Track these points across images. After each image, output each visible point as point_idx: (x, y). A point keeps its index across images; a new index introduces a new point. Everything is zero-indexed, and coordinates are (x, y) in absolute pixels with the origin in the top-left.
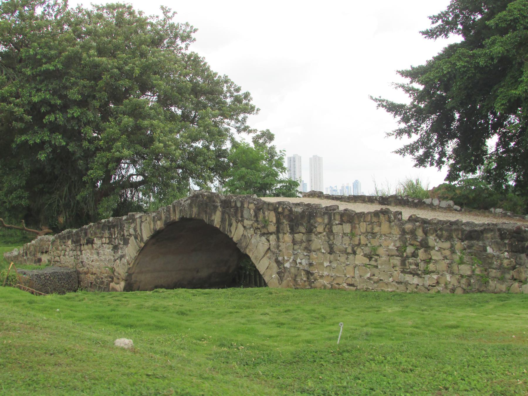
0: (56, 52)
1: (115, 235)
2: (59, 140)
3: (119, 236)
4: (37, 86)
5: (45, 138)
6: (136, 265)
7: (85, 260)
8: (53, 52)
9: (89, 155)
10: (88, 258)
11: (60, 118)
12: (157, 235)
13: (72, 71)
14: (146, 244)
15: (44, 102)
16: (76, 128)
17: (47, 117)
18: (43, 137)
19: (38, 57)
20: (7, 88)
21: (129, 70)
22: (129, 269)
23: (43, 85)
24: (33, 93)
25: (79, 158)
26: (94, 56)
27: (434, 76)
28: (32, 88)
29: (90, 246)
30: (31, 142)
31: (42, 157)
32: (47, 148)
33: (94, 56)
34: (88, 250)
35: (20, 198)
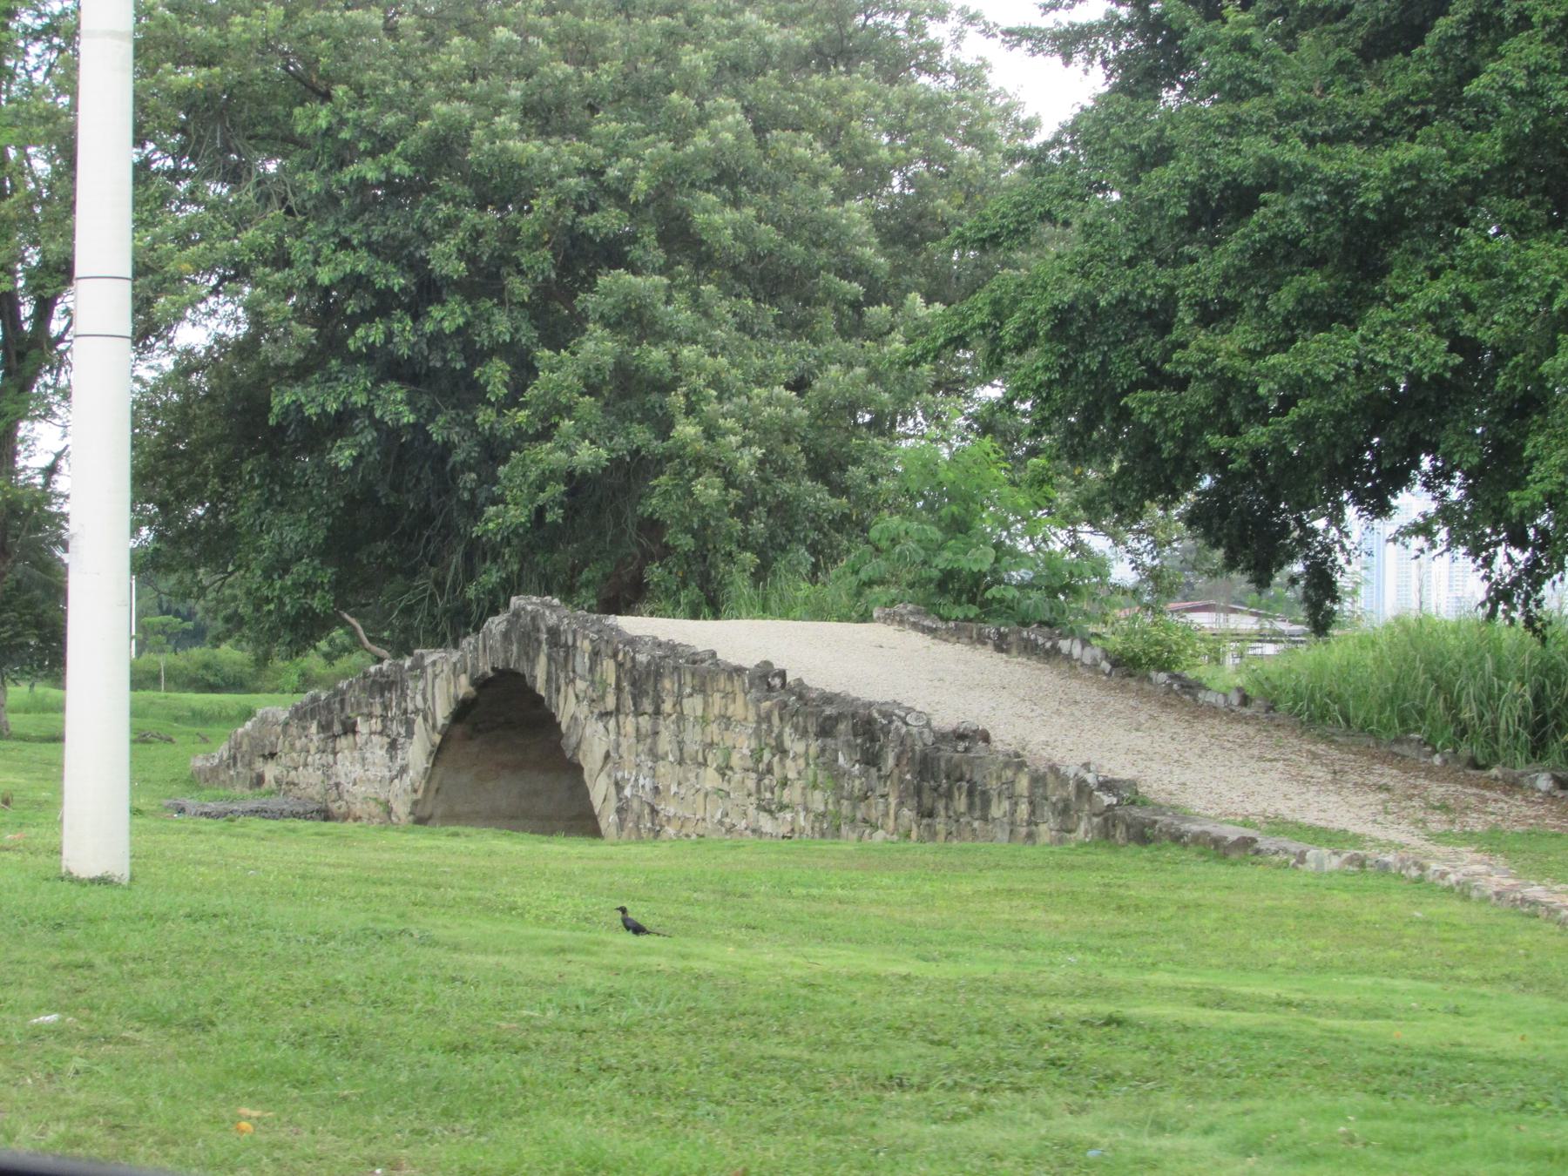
0: (402, 116)
2: (396, 405)
4: (341, 230)
5: (354, 399)
6: (432, 793)
7: (343, 780)
8: (390, 119)
9: (494, 451)
11: (404, 334)
12: (463, 711)
13: (442, 182)
14: (446, 736)
15: (355, 283)
16: (458, 366)
17: (360, 332)
18: (350, 395)
19: (345, 134)
21: (619, 179)
22: (415, 803)
23: (358, 226)
24: (326, 252)
25: (466, 466)
26: (507, 134)
27: (924, 347)
28: (325, 237)
29: (350, 737)
30: (311, 411)
31: (343, 456)
32: (362, 431)
33: (507, 134)
35: (309, 587)
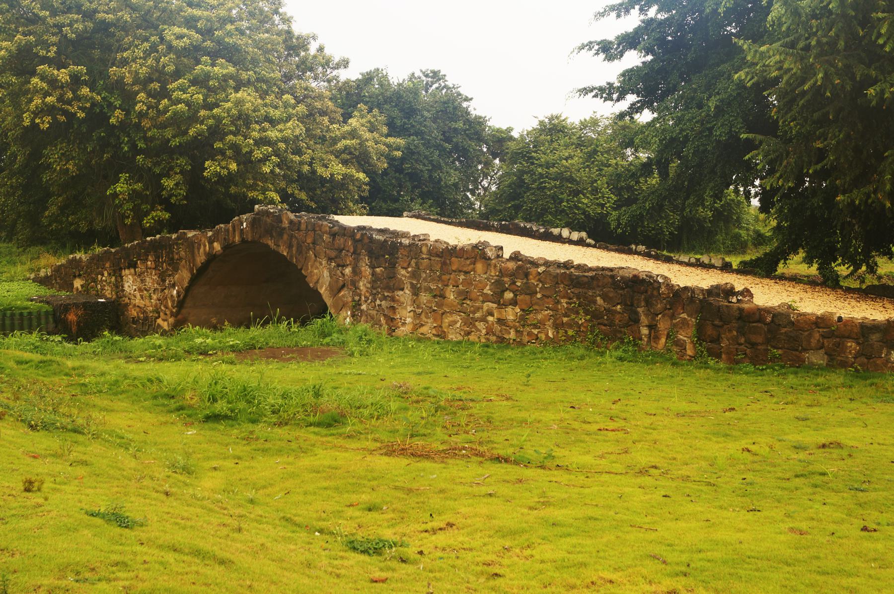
29: (132, 270)
34: (130, 277)
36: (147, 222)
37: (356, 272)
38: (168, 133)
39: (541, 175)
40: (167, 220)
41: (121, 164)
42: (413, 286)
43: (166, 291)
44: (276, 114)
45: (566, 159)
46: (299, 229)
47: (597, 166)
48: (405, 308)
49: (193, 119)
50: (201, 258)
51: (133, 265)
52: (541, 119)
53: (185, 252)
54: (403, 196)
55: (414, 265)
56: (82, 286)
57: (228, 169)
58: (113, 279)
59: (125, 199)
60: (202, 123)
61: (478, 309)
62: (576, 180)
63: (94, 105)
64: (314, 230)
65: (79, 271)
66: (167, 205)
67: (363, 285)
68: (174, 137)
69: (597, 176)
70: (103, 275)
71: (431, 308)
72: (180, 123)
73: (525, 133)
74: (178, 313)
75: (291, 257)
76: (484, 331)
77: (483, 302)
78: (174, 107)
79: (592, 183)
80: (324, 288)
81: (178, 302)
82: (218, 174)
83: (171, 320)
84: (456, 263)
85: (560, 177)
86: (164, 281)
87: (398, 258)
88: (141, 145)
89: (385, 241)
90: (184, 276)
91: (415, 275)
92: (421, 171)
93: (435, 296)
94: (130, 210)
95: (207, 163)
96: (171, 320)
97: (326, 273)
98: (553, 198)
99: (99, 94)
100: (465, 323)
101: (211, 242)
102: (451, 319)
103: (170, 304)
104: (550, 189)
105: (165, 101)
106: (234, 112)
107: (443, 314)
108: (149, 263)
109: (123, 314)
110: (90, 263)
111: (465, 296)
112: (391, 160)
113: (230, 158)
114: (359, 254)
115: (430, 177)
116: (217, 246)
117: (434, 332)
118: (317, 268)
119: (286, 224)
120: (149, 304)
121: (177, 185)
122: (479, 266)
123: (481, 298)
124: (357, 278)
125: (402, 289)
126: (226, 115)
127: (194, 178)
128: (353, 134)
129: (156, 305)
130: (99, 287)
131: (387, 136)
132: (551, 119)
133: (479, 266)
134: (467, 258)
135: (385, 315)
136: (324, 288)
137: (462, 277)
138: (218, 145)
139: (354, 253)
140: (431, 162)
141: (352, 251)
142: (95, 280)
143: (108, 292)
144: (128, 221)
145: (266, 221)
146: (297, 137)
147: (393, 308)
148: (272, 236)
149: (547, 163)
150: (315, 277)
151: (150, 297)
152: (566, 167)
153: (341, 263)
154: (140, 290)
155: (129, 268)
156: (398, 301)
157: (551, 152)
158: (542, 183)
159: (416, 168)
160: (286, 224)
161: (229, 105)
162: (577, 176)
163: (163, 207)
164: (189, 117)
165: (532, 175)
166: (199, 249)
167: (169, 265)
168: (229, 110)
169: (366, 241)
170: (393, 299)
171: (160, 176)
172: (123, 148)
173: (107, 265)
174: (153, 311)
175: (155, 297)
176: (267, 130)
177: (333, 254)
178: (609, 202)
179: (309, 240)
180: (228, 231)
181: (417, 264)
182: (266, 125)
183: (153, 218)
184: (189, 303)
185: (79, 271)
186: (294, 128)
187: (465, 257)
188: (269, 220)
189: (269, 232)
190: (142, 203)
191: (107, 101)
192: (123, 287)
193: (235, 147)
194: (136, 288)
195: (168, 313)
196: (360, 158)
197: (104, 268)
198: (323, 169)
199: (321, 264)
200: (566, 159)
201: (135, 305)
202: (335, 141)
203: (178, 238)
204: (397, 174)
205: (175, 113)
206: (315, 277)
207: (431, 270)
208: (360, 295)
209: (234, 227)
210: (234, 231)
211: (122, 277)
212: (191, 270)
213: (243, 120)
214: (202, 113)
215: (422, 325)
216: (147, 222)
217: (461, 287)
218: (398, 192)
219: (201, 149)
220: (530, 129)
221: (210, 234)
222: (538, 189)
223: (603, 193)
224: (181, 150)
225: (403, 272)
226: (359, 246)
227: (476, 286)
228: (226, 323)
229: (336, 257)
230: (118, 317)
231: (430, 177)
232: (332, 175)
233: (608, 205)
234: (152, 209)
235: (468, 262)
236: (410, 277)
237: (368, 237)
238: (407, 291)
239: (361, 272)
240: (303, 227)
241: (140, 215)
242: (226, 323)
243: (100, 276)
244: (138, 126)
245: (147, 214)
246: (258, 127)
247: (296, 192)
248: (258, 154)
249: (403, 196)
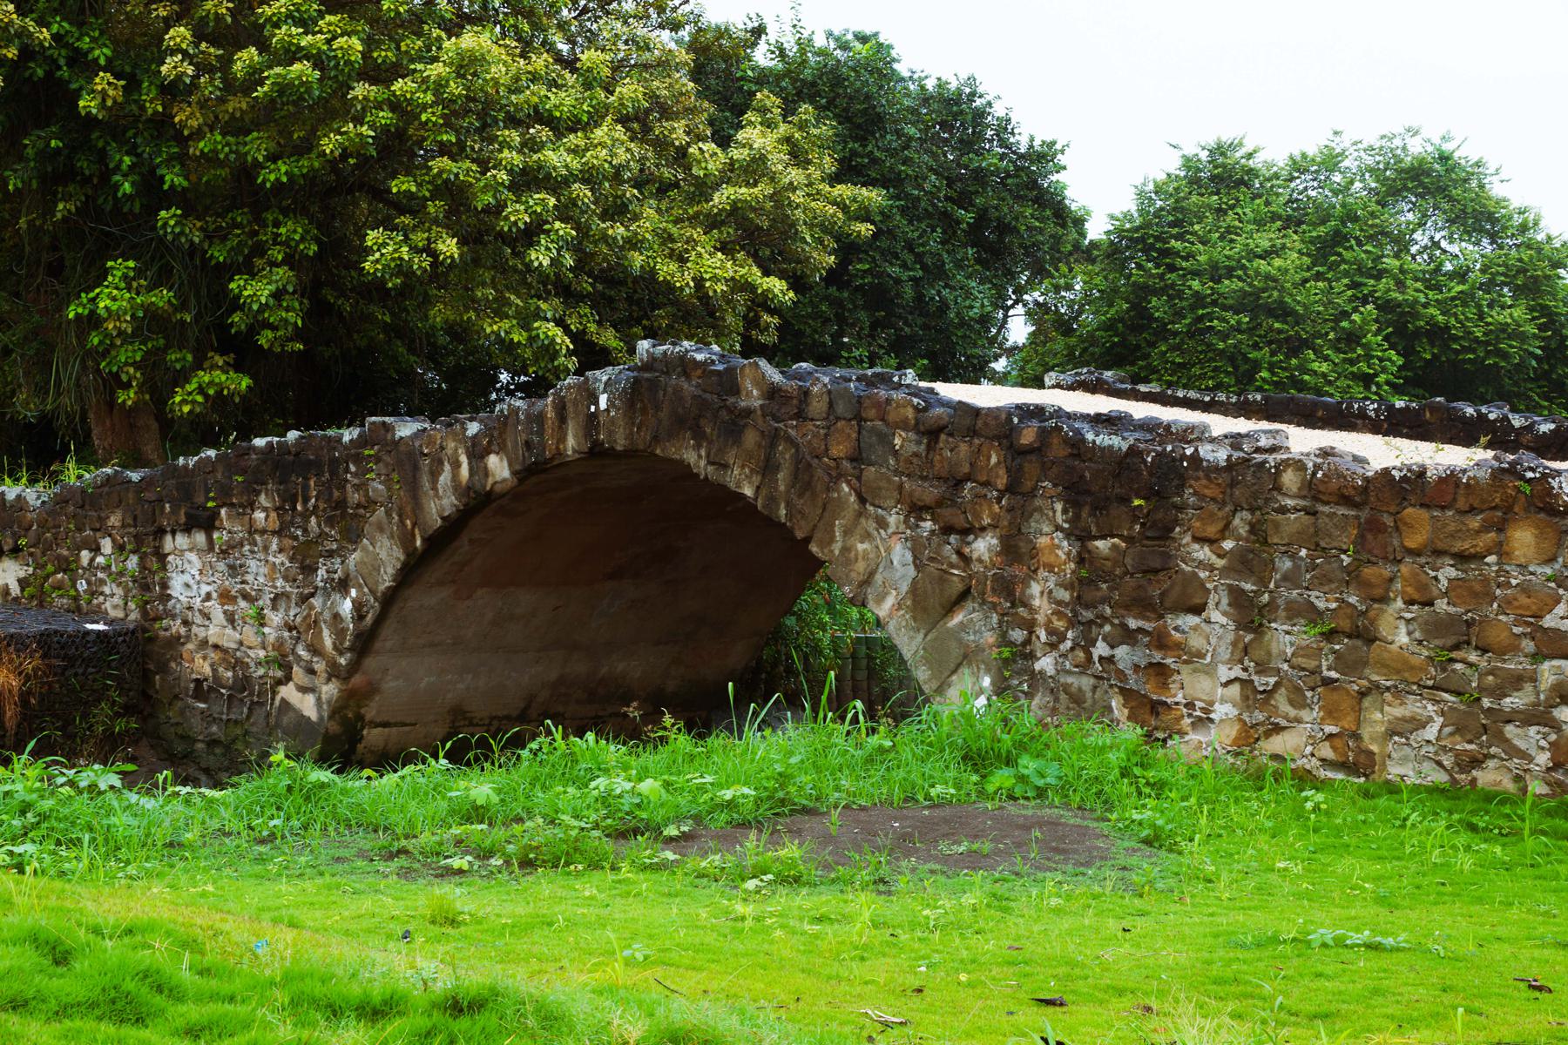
1: (306, 500)
3: (322, 506)
10: (187, 585)
20: (1036, 294)
29: (200, 538)
34: (193, 556)
36: (184, 401)
37: (1015, 549)
38: (257, 146)
39: (1199, 299)
40: (243, 398)
41: (107, 232)
42: (1239, 600)
43: (317, 602)
44: (563, 101)
45: (1266, 255)
46: (801, 415)
47: (1346, 274)
48: (1210, 671)
49: (334, 107)
50: (441, 502)
51: (208, 523)
52: (1190, 150)
53: (388, 482)
54: (848, 347)
55: (1243, 531)
56: (23, 583)
57: (434, 254)
58: (133, 562)
59: (121, 333)
60: (358, 120)
61: (1517, 681)
62: (1293, 313)
63: (27, 53)
64: (859, 418)
65: (16, 537)
66: (242, 352)
67: (1041, 594)
68: (273, 158)
69: (1350, 300)
70: (96, 550)
71: (1315, 672)
72: (299, 118)
73: (1151, 187)
74: (354, 667)
75: (772, 500)
76: (1543, 759)
77: (1538, 657)
78: (278, 70)
79: (1337, 320)
80: (890, 601)
81: (358, 636)
82: (402, 269)
83: (330, 690)
84: (1419, 526)
85: (1249, 303)
86: (309, 570)
87: (1181, 508)
88: (173, 178)
89: (1133, 451)
90: (382, 555)
91: (1247, 563)
92: (898, 281)
93: (1330, 636)
94: (134, 364)
95: (372, 236)
96: (330, 690)
97: (900, 554)
98: (1232, 360)
99: (41, 23)
100: (1460, 725)
101: (478, 453)
102: (1398, 712)
103: (328, 641)
104: (1224, 337)
105: (248, 56)
106: (455, 88)
107: (1362, 694)
108: (259, 516)
109: (164, 669)
110: (52, 513)
111: (1457, 635)
112: (848, 249)
113: (436, 222)
114: (1032, 494)
115: (920, 297)
116: (499, 467)
117: (1327, 751)
118: (867, 536)
119: (752, 397)
120: (254, 644)
121: (277, 295)
122: (1523, 538)
123: (1528, 646)
124: (1018, 571)
125: (1198, 610)
126: (429, 98)
127: (328, 273)
128: (755, 169)
129: (279, 645)
130: (82, 585)
131: (835, 179)
132: (1219, 150)
133: (1523, 538)
134: (1472, 510)
135: (1127, 693)
136: (890, 601)
137: (1447, 573)
138: (401, 185)
139: (1010, 489)
140: (919, 258)
141: (1002, 481)
142: (67, 566)
143: (118, 603)
144: (127, 397)
145: (678, 391)
146: (618, 170)
147: (1161, 672)
148: (699, 436)
149: (1214, 266)
150: (861, 566)
151: (261, 620)
152: (1268, 277)
153: (959, 521)
154: (226, 597)
155: (187, 530)
156: (1179, 647)
157: (1222, 238)
158: (1200, 319)
159: (881, 275)
160: (752, 397)
161: (436, 70)
162: (1298, 300)
163: (231, 358)
164: (323, 102)
165: (1171, 298)
166: (435, 475)
167: (331, 522)
168: (439, 86)
169: (1058, 450)
170: (1161, 641)
171: (226, 271)
172: (117, 186)
173: (114, 520)
174: (268, 662)
175: (275, 618)
176: (542, 146)
177: (930, 492)
178: (1384, 370)
179: (839, 449)
180: (540, 418)
181: (1253, 529)
182: (542, 133)
183: (201, 390)
184: (389, 637)
185: (16, 537)
186: (610, 145)
187: (1462, 503)
188: (689, 388)
189: (689, 422)
190: (167, 347)
191: (67, 45)
192: (165, 585)
193: (454, 193)
194: (218, 596)
195: (320, 666)
196: (758, 235)
197: (102, 529)
198: (673, 266)
199: (882, 524)
200: (1266, 255)
201: (204, 643)
202: (704, 188)
203: (362, 442)
204: (833, 290)
205: (283, 88)
206: (861, 566)
207: (1316, 548)
208: (1030, 626)
209: (561, 408)
210: (562, 418)
211: (162, 558)
212: (406, 540)
213: (480, 114)
214: (360, 90)
215: (1278, 729)
216: (184, 401)
217: (1442, 605)
218: (836, 337)
219: (348, 193)
220: (1162, 177)
221: (473, 428)
222: (1190, 334)
223: (1367, 347)
224: (293, 198)
225: (1203, 553)
226: (1031, 467)
227: (1508, 601)
228: (668, 720)
229: (940, 503)
230: (146, 676)
231: (920, 297)
232: (699, 282)
233: (1382, 378)
234: (198, 365)
235: (1475, 522)
236: (1224, 572)
237: (1066, 441)
238: (1216, 616)
239: (1034, 552)
240: (817, 406)
241: (161, 381)
242: (668, 720)
243: (85, 555)
244: (162, 126)
245: (182, 377)
246: (515, 136)
247: (592, 327)
248: (517, 214)
249: (848, 347)
